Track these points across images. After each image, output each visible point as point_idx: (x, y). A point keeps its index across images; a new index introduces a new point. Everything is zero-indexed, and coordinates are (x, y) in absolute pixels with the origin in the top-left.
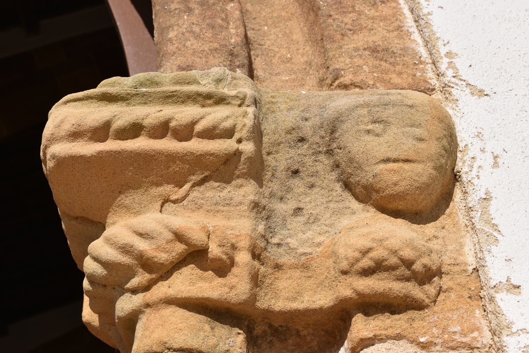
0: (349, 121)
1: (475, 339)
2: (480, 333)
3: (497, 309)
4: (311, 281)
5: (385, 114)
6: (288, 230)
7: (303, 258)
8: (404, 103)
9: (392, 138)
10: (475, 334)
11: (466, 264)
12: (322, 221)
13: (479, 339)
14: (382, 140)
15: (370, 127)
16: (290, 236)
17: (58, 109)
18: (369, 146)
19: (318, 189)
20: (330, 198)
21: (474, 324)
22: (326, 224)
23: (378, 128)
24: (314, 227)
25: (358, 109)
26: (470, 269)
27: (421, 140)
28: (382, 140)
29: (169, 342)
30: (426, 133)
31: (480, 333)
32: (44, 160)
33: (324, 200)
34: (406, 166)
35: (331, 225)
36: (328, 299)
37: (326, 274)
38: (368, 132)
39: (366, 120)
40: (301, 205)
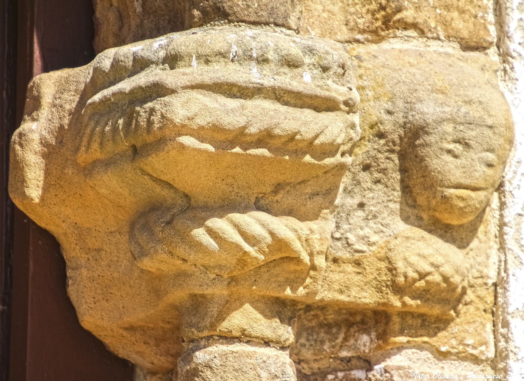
0: (434, 135)
1: (482, 352)
2: (487, 347)
3: (510, 335)
4: (359, 277)
5: (470, 134)
6: (350, 224)
7: (357, 255)
8: (497, 233)
9: (468, 164)
10: (483, 348)
11: (488, 277)
12: (379, 219)
13: (486, 353)
14: (459, 163)
15: (451, 146)
16: (350, 230)
17: (186, 90)
18: (447, 168)
19: (382, 186)
20: (391, 198)
21: (484, 338)
22: (383, 223)
23: (458, 148)
24: (371, 223)
25: (445, 123)
26: (490, 282)
27: (490, 165)
28: (459, 163)
29: (249, 330)
30: (496, 159)
31: (487, 347)
32: (331, 332)
33: (385, 199)
34: (473, 194)
35: (386, 226)
36: (373, 300)
37: (375, 274)
38: (449, 152)
39: (450, 138)
40: (365, 200)
